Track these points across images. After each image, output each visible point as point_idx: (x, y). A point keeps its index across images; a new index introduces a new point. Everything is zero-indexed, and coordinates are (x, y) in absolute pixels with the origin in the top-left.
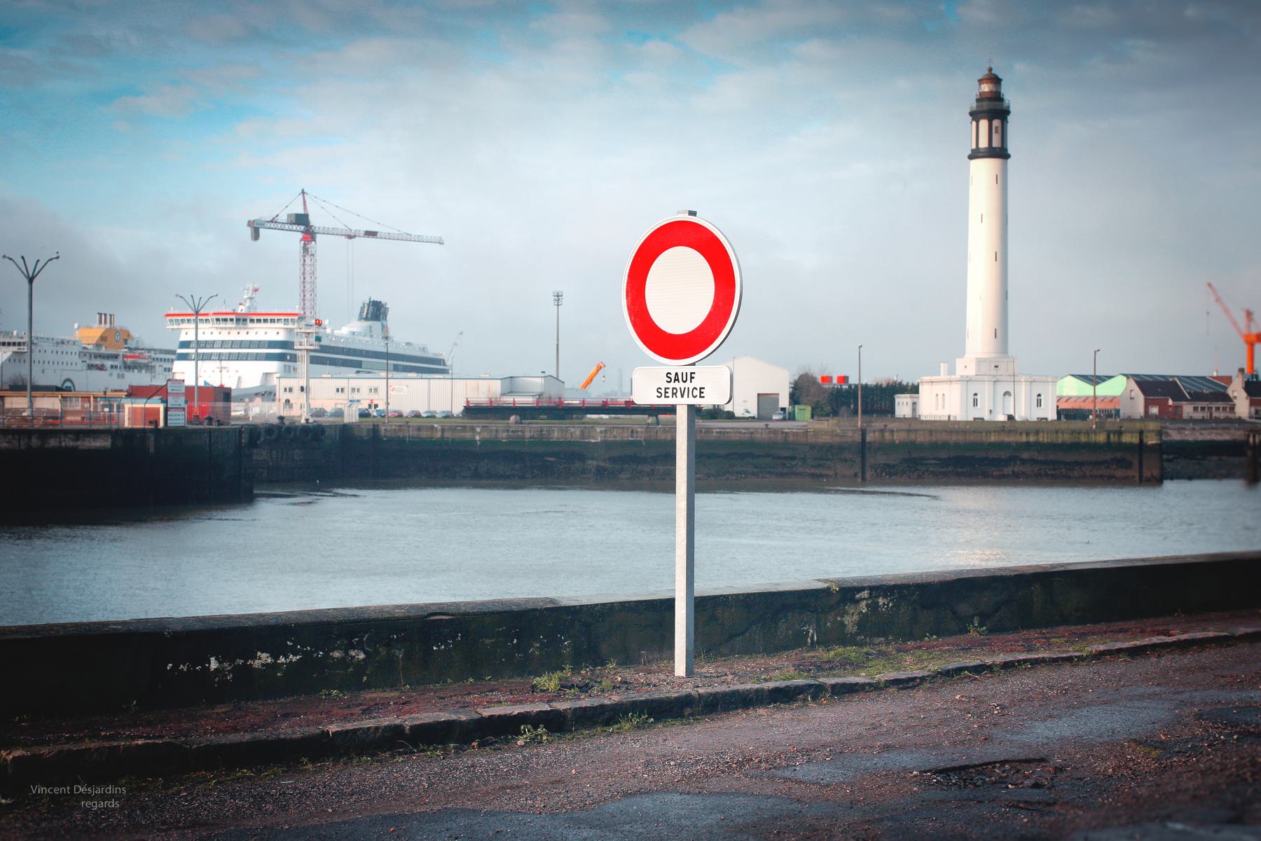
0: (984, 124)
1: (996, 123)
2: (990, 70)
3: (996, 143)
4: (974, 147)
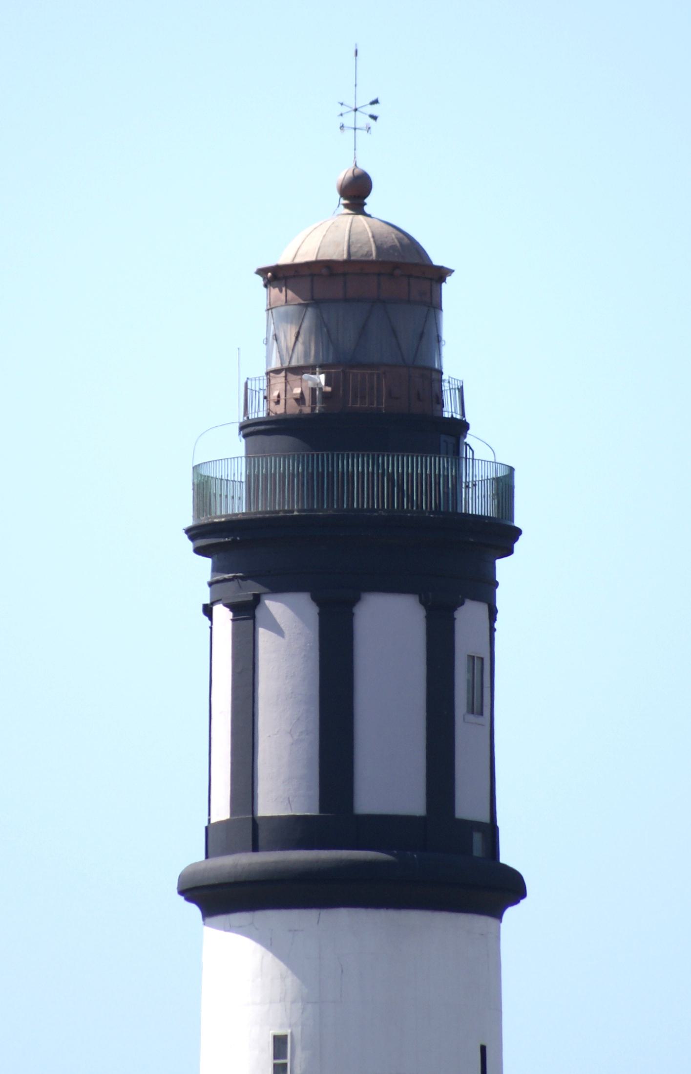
0: (288, 627)
1: (389, 623)
2: (356, 191)
3: (389, 785)
4: (222, 812)
